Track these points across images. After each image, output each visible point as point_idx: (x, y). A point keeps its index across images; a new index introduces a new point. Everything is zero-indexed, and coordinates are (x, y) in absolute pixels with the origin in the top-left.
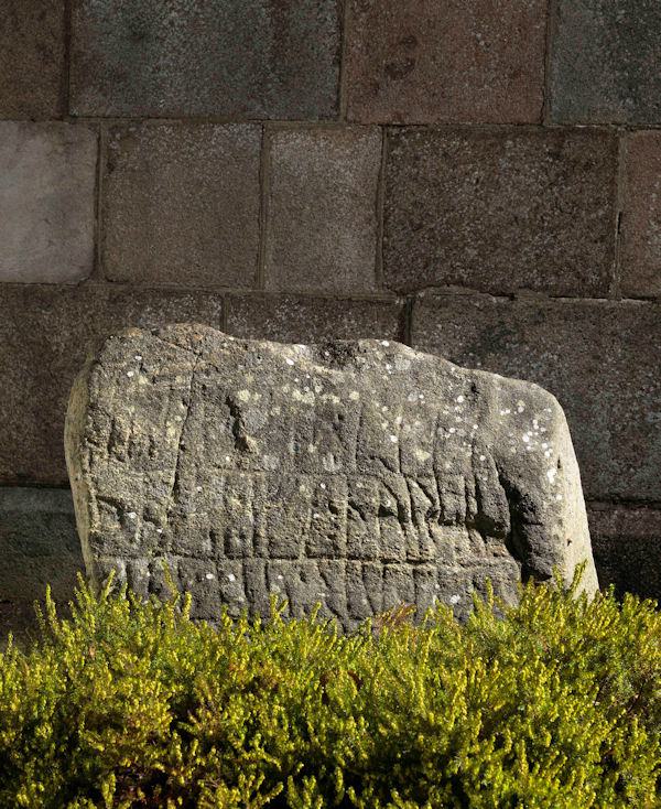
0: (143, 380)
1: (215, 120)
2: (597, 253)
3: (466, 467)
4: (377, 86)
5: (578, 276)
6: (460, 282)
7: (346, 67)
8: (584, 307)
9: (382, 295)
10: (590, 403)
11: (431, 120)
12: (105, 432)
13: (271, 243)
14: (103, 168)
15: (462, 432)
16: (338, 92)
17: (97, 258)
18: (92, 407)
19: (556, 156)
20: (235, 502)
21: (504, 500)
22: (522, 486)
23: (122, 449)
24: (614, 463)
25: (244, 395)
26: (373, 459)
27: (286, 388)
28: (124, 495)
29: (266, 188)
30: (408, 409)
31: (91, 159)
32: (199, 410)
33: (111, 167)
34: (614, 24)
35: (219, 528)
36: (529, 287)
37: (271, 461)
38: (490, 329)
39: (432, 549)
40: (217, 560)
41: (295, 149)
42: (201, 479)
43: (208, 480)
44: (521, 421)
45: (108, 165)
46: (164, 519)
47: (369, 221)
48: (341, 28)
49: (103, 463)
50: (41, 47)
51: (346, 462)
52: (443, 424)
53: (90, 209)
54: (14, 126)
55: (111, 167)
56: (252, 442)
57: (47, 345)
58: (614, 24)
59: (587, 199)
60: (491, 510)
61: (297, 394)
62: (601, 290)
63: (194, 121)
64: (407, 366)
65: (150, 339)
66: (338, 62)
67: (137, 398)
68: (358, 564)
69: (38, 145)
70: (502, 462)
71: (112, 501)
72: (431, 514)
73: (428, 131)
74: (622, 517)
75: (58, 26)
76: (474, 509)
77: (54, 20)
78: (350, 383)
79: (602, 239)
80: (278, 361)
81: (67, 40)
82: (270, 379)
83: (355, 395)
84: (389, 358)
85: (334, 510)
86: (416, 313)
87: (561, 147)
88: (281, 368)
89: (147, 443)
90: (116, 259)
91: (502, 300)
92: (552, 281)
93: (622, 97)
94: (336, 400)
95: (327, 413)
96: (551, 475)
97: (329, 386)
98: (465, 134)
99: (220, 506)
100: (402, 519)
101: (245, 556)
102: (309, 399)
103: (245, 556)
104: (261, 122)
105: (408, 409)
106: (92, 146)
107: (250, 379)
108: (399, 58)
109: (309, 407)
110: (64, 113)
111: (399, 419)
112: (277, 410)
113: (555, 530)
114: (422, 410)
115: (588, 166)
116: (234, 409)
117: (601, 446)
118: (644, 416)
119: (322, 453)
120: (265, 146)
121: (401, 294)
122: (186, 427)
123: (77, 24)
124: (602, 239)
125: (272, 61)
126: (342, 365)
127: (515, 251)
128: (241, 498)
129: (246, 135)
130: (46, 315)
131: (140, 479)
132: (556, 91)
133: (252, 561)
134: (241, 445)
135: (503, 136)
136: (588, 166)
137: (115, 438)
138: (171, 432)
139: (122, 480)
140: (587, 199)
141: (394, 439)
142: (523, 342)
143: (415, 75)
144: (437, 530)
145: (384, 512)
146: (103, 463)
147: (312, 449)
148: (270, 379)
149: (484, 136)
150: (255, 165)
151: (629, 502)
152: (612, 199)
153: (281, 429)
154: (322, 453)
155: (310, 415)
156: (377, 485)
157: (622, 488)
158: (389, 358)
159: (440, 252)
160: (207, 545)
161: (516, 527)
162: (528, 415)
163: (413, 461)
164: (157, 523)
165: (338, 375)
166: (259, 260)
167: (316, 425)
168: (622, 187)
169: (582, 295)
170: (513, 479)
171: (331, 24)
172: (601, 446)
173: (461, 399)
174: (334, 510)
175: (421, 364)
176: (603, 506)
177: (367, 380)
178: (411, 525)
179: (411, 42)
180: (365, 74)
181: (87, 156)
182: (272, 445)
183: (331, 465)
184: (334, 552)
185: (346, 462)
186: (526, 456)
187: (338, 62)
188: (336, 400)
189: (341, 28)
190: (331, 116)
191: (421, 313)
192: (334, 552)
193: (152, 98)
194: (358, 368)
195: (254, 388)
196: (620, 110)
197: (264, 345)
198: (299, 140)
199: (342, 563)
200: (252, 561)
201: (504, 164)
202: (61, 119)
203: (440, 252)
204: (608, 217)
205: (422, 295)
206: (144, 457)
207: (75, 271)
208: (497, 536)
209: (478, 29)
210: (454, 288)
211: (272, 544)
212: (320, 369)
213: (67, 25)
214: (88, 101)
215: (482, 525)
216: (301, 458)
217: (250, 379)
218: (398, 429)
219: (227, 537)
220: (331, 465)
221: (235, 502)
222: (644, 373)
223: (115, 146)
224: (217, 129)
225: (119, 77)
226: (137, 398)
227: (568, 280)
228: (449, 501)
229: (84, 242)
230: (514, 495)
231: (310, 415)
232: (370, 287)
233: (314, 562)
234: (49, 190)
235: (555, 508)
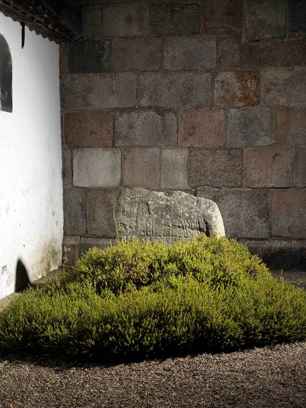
0: (129, 199)
1: (149, 147)
2: (239, 177)
3: (196, 217)
4: (187, 138)
5: (235, 183)
6: (208, 185)
7: (179, 134)
8: (237, 191)
9: (190, 189)
10: (240, 214)
11: (200, 146)
12: (122, 210)
13: (163, 176)
14: (123, 159)
15: (195, 210)
16: (178, 139)
17: (122, 181)
18: (119, 204)
19: (229, 154)
20: (148, 224)
21: (204, 224)
22: (208, 221)
23: (125, 213)
24: (246, 229)
25: (150, 202)
26: (177, 216)
27: (159, 201)
28: (125, 223)
29: (161, 164)
30: (184, 205)
31: (120, 157)
32: (141, 205)
33: (125, 159)
34: (241, 123)
35: (145, 229)
36: (224, 186)
37: (155, 216)
38: (215, 196)
39: (189, 234)
40: (145, 237)
41: (168, 154)
42: (141, 220)
43: (143, 220)
44: (208, 208)
45: (124, 158)
46: (134, 228)
47: (186, 170)
48: (178, 125)
49: (121, 216)
50: (108, 130)
51: (171, 216)
52: (192, 208)
53: (120, 169)
54: (102, 149)
55: (125, 159)
56: (152, 212)
57: (110, 203)
58: (241, 123)
59: (237, 165)
60: (202, 226)
61: (161, 202)
62: (241, 186)
63: (144, 147)
64: (184, 196)
65: (131, 191)
66: (177, 133)
67: (128, 203)
68: (174, 238)
69: (108, 153)
70: (204, 216)
71: (123, 224)
72: (189, 227)
73: (199, 149)
74: (248, 243)
75: (112, 125)
76: (198, 226)
77: (111, 124)
78: (172, 200)
79: (241, 174)
80: (157, 195)
81: (114, 128)
82: (155, 199)
83: (173, 202)
84: (180, 195)
85: (169, 226)
86: (197, 193)
87: (230, 152)
88: (158, 197)
89: (130, 212)
90: (126, 181)
91: (218, 189)
92: (229, 184)
93: (244, 140)
94: (169, 203)
95: (167, 206)
96: (214, 219)
97: (167, 201)
98: (207, 149)
99: (145, 225)
100: (183, 228)
101: (150, 236)
102: (163, 203)
103: (150, 236)
104: (160, 147)
105: (184, 205)
106: (120, 154)
107: (151, 199)
108: (191, 131)
109: (163, 205)
110: (113, 146)
111: (182, 208)
112: (157, 205)
113: (215, 231)
114: (187, 206)
115: (236, 156)
116: (148, 206)
117: (243, 225)
118: (252, 217)
119: (166, 214)
120: (161, 153)
121: (194, 188)
122: (138, 209)
123: (116, 125)
124: (241, 174)
125: (162, 132)
126: (170, 196)
127: (220, 177)
128: (150, 223)
129: (156, 150)
130: (110, 195)
131: (129, 219)
132: (228, 139)
133: (152, 237)
134: (150, 212)
135: (216, 150)
136: (236, 156)
137: (124, 211)
138: (135, 210)
139: (126, 220)
140: (237, 165)
141: (181, 211)
142: (223, 200)
143: (195, 136)
144: (190, 230)
145: (179, 227)
146: (121, 216)
147: (164, 213)
148: (155, 199)
149: (212, 150)
150: (158, 158)
151: (250, 239)
152: (242, 164)
153: (157, 210)
154: (166, 214)
155: (164, 206)
156: (178, 221)
157: (248, 235)
158: (180, 195)
159: (203, 178)
160: (143, 233)
161: (207, 230)
162: (209, 206)
163: (185, 216)
164: (132, 228)
165: (169, 198)
166: (160, 180)
167: (165, 209)
168: (245, 161)
169: (236, 188)
170: (206, 220)
171: (175, 124)
172: (243, 225)
173: (195, 203)
174: (169, 226)
175: (187, 196)
176: (244, 240)
177: (175, 199)
178: (185, 229)
179: (194, 127)
180: (184, 135)
181: (119, 156)
182: (156, 213)
183: (168, 217)
184: (169, 235)
185: (171, 216)
186: (209, 215)
187: (177, 133)
188: (169, 203)
189: (178, 125)
190: (176, 146)
191: (198, 193)
192: (169, 235)
193: (134, 142)
194: (173, 197)
195: (152, 201)
196: (244, 143)
197: (154, 192)
198: (169, 151)
199: (171, 237)
200: (152, 237)
201: (217, 156)
202: (113, 147)
203: (203, 178)
204: (242, 168)
205: (199, 188)
206: (129, 215)
207: (117, 184)
208: (204, 232)
209: (210, 124)
210: (207, 187)
211: (156, 233)
212: (166, 197)
213: (114, 125)
214: (119, 143)
215: (200, 230)
216: (162, 215)
217: (151, 199)
218: (182, 209)
219: (147, 232)
220: (168, 217)
221: (148, 224)
222: (252, 207)
223: (125, 153)
224: (149, 149)
225: (127, 137)
226: (128, 203)
227: (233, 184)
228: (193, 225)
229: (119, 177)
230: (206, 223)
231: (164, 206)
232: (187, 187)
233: (165, 237)
234: (110, 165)
235: (215, 226)
